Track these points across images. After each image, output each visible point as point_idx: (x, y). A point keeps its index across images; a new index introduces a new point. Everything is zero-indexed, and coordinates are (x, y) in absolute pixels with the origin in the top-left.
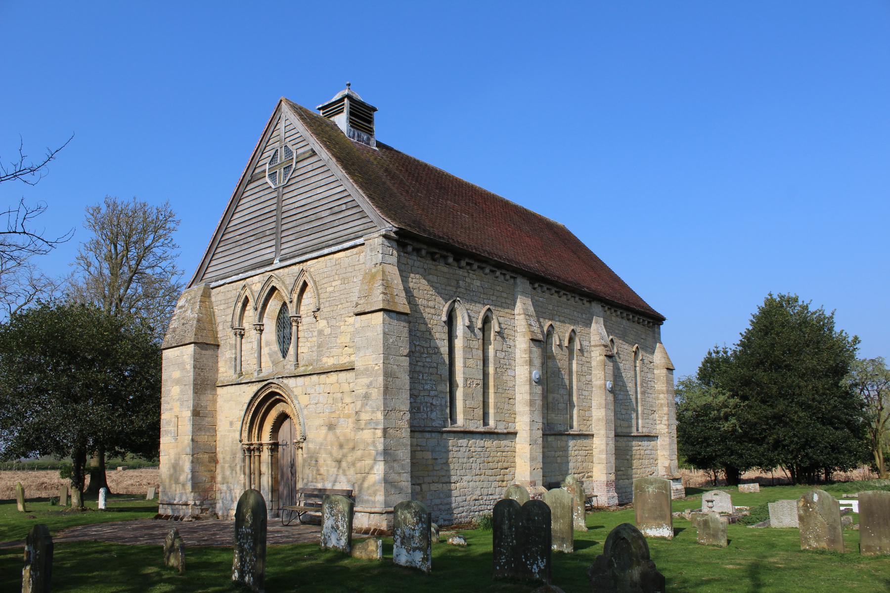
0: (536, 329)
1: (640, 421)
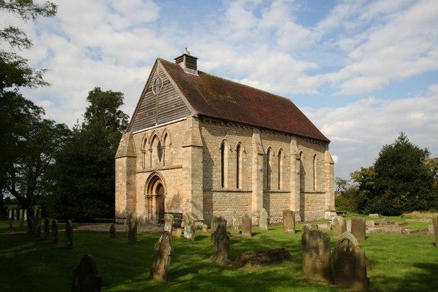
0: (261, 149)
1: (315, 186)
